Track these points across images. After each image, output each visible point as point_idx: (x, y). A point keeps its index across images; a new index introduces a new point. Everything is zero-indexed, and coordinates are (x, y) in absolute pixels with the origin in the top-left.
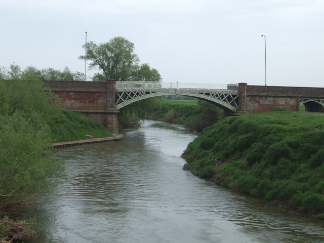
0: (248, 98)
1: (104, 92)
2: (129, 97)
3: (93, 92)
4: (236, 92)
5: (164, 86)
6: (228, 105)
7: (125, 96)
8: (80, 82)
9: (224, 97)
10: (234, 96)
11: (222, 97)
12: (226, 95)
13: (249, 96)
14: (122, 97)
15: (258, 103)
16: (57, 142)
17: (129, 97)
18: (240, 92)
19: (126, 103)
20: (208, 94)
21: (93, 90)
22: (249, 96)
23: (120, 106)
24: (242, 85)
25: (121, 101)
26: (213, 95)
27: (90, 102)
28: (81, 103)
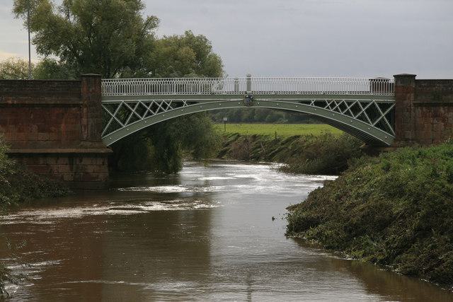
0: (419, 110)
1: (74, 106)
2: (134, 115)
3: (48, 105)
4: (388, 97)
5: (228, 88)
6: (370, 129)
7: (141, 110)
8: (165, 194)
9: (346, 108)
10: (384, 106)
11: (356, 109)
12: (364, 104)
13: (421, 105)
14: (151, 109)
15: (443, 121)
16: (106, 111)
17: (134, 115)
18: (400, 98)
19: (127, 130)
20: (321, 104)
21: (51, 100)
22: (421, 105)
23: (113, 138)
24: (405, 80)
25: (115, 126)
26: (333, 105)
27: (41, 130)
28: (20, 131)
